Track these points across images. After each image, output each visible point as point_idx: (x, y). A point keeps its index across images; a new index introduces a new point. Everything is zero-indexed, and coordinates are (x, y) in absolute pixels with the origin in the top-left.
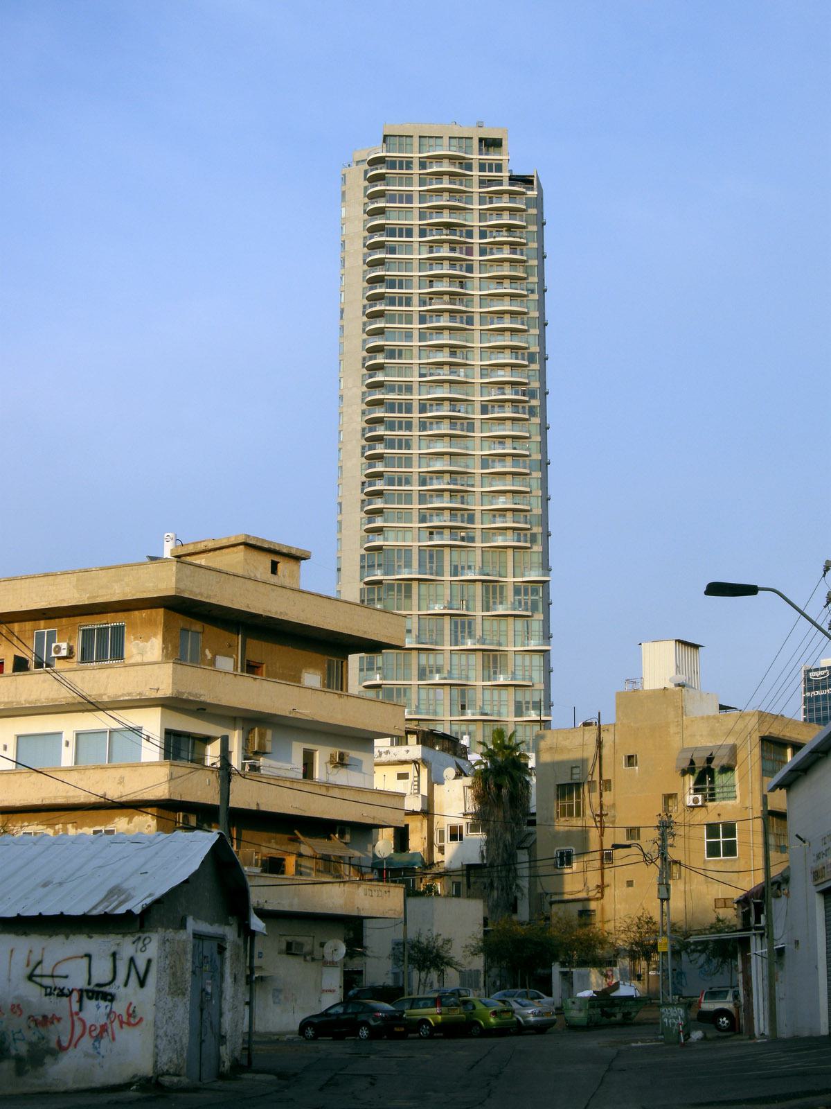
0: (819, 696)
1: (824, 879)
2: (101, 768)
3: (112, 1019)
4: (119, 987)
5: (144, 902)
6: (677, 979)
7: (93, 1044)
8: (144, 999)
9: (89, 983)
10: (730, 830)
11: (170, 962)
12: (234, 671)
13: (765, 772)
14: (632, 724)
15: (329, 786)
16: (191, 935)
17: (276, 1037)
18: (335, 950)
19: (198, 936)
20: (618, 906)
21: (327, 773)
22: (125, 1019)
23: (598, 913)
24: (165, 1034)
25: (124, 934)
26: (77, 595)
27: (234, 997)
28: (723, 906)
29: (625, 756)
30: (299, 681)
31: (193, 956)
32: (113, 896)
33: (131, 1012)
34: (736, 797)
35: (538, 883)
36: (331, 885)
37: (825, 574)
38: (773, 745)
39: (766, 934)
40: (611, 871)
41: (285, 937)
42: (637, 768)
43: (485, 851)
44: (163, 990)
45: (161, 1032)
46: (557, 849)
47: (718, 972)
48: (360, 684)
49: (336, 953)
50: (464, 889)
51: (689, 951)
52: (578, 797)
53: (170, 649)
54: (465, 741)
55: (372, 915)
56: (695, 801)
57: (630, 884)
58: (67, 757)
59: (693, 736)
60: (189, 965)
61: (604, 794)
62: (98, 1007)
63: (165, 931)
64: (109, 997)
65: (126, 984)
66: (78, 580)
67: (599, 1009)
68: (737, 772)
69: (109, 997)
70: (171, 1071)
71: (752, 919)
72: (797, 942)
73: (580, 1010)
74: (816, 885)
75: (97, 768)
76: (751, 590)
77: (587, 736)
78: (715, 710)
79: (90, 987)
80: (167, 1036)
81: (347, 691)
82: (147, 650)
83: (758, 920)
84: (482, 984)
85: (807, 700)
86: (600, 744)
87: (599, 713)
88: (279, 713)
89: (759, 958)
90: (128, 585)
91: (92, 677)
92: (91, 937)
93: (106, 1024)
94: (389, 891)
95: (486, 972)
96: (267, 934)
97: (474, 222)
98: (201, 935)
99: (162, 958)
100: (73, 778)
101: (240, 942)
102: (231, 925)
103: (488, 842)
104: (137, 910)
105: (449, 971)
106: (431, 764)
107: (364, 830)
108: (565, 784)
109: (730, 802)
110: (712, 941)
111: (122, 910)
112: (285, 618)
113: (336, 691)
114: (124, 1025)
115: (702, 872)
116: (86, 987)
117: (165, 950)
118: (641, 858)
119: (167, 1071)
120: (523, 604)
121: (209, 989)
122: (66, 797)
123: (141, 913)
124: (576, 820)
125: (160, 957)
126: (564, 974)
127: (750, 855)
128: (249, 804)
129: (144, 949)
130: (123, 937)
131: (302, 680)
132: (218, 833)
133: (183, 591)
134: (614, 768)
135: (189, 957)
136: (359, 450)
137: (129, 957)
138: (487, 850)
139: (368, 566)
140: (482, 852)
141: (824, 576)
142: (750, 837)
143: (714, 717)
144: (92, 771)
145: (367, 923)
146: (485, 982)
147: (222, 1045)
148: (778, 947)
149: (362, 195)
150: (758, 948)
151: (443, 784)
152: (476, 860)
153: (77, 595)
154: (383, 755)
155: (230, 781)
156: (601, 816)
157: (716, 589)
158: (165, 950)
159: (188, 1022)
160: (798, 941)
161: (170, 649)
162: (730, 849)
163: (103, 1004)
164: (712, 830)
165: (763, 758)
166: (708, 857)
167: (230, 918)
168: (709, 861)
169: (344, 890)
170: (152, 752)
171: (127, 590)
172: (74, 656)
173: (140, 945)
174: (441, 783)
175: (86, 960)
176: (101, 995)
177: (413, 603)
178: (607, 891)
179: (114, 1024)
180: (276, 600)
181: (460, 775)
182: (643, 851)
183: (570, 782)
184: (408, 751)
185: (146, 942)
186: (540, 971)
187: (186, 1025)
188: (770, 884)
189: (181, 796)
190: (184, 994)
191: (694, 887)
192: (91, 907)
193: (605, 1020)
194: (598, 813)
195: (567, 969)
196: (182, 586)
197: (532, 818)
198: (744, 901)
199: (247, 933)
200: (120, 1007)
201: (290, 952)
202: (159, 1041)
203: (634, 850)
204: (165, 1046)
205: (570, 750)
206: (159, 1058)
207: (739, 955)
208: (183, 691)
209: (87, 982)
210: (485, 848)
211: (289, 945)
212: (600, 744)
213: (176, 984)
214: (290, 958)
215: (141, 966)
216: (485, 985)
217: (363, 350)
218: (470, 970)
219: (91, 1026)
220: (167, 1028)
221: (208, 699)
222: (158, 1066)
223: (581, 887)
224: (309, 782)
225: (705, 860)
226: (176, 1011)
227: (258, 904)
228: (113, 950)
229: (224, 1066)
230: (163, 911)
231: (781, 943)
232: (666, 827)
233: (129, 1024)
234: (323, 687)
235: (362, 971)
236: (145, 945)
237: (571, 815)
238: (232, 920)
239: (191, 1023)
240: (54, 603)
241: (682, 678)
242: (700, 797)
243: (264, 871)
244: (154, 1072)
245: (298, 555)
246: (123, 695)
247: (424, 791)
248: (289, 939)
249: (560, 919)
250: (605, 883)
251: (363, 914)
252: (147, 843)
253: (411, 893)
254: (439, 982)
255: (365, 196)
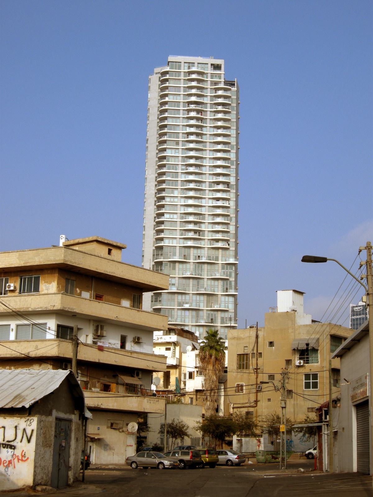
0: (358, 318)
1: (356, 400)
2: (27, 341)
3: (14, 458)
4: (18, 443)
5: (30, 403)
6: (290, 444)
7: (5, 470)
8: (30, 449)
9: (4, 441)
10: (315, 376)
11: (43, 432)
12: (90, 298)
13: (332, 351)
14: (272, 328)
15: (132, 352)
16: (55, 419)
17: (104, 467)
18: (133, 427)
19: (58, 419)
20: (264, 410)
21: (131, 346)
22: (20, 458)
23: (254, 413)
24: (40, 465)
25: (21, 418)
26: (18, 262)
27: (76, 448)
28: (311, 411)
29: (268, 342)
30: (120, 304)
31: (56, 428)
32: (17, 399)
33: (23, 454)
34: (318, 362)
35: (228, 398)
36: (132, 397)
37: (359, 253)
38: (336, 339)
39: (329, 424)
40: (261, 394)
41: (110, 421)
42: (274, 347)
43: (204, 384)
44: (39, 444)
45: (38, 465)
46: (237, 383)
47: (307, 441)
48: (151, 307)
49: (133, 428)
50: (194, 400)
51: (295, 431)
52: (247, 360)
53: (60, 288)
54: (197, 334)
55: (150, 412)
56: (300, 363)
57: (269, 400)
58: (12, 336)
59: (299, 333)
60: (53, 433)
61: (259, 359)
62: (8, 452)
63: (41, 417)
64: (13, 447)
65: (21, 441)
66: (19, 255)
67: (271, 456)
68: (319, 352)
69: (13, 447)
70: (43, 483)
71: (323, 417)
72: (343, 429)
73: (263, 456)
74: (353, 402)
75: (26, 341)
76: (324, 260)
77: (251, 333)
78: (309, 322)
79: (4, 442)
80: (40, 466)
81: (142, 309)
82: (50, 288)
83: (326, 418)
84: (201, 444)
85: (353, 320)
86: (257, 337)
87: (257, 322)
88: (109, 318)
89: (326, 436)
90: (42, 258)
91: (24, 299)
92: (5, 418)
93: (11, 460)
94: (158, 401)
95: (203, 438)
96: (93, 419)
97: (206, 100)
98: (60, 419)
99: (39, 430)
100: (14, 346)
101: (80, 422)
102: (75, 414)
103: (205, 380)
104: (27, 406)
105: (186, 438)
106: (181, 344)
107: (148, 373)
108: (241, 354)
109: (316, 364)
110: (305, 427)
111: (20, 406)
112: (114, 275)
113: (136, 309)
114: (20, 461)
115: (302, 395)
116: (2, 442)
117: (41, 425)
118: (273, 388)
119: (40, 483)
120: (226, 273)
121: (64, 444)
122: (11, 354)
123: (29, 407)
124: (246, 371)
125: (38, 429)
126: (238, 440)
127: (324, 389)
128: (95, 360)
129: (30, 425)
130: (21, 419)
131: (121, 303)
132: (70, 371)
133: (67, 261)
134: (263, 347)
135: (53, 429)
136: (154, 203)
137: (23, 429)
138: (205, 383)
139: (156, 255)
140: (203, 384)
141: (359, 254)
142: (324, 379)
143: (309, 325)
144: (23, 342)
145: (149, 415)
146: (202, 443)
147: (70, 471)
148: (334, 430)
149: (158, 88)
150: (325, 431)
151: (186, 353)
152: (200, 388)
153: (18, 262)
154: (159, 339)
155: (78, 347)
156: (257, 369)
157: (307, 259)
158: (41, 425)
159: (52, 460)
160: (344, 428)
161: (60, 288)
162: (315, 385)
163: (10, 450)
164: (307, 376)
165: (331, 345)
166: (305, 389)
167: (75, 411)
168: (306, 391)
169: (138, 400)
170: (51, 334)
171: (41, 260)
172: (16, 290)
173: (29, 423)
174: (185, 352)
175: (3, 429)
176: (9, 446)
177: (176, 272)
178: (259, 403)
179: (15, 460)
180: (110, 266)
181: (194, 349)
182: (274, 385)
183: (243, 353)
184: (170, 338)
185: (31, 421)
186: (227, 438)
187: (51, 462)
188: (331, 401)
189: (64, 355)
190: (50, 447)
191: (298, 402)
192: (5, 404)
193: (273, 460)
194: (256, 368)
195: (240, 438)
196: (67, 259)
197: (226, 369)
198: (320, 409)
199: (84, 419)
200: (18, 452)
201: (112, 427)
202: (37, 469)
203: (270, 384)
204: (39, 471)
205: (243, 339)
206: (36, 477)
207: (317, 434)
208: (66, 307)
209: (3, 440)
210: (204, 382)
211: (112, 424)
212: (257, 337)
213: (46, 442)
214: (113, 431)
215: (29, 432)
216: (202, 445)
217: (156, 158)
218: (196, 438)
219: (4, 461)
220: (40, 463)
221: (77, 311)
222: (36, 481)
223: (247, 401)
224: (123, 350)
225: (303, 390)
226: (46, 454)
227: (98, 405)
228: (15, 424)
229: (70, 481)
230: (39, 408)
231: (337, 428)
232: (285, 374)
233: (22, 460)
234: (131, 307)
235: (147, 437)
236: (31, 423)
237: (243, 368)
238: (76, 412)
239: (53, 460)
240: (8, 265)
241: (294, 307)
242: (302, 361)
243: (101, 390)
244: (33, 483)
245: (121, 246)
246: (38, 308)
247: (177, 355)
248: (112, 421)
249: (237, 415)
250: (258, 400)
251: (146, 411)
252: (35, 374)
253: (168, 402)
254: (181, 443)
255: (159, 89)
